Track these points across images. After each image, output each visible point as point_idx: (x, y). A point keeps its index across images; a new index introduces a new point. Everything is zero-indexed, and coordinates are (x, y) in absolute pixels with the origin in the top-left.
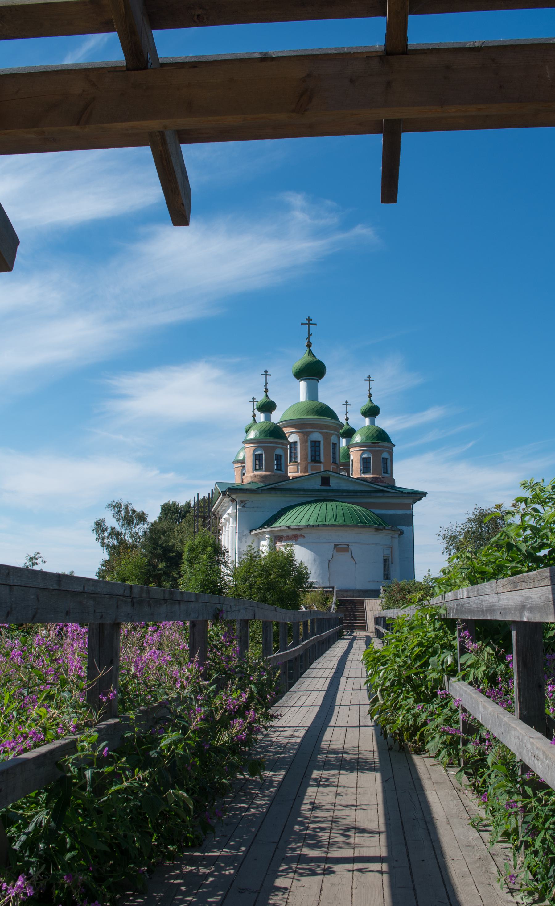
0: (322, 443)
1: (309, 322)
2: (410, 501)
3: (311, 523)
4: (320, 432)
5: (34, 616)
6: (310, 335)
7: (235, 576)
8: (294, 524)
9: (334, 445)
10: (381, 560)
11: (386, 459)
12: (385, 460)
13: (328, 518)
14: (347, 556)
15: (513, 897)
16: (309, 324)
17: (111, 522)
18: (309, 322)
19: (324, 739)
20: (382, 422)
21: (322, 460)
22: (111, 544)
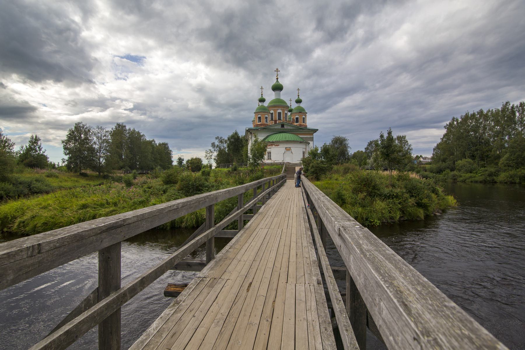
0: (282, 113)
1: (262, 88)
2: (312, 133)
3: (277, 140)
4: (281, 109)
5: (98, 290)
6: (278, 75)
7: (309, 154)
8: (272, 140)
9: (286, 114)
10: (302, 153)
11: (304, 118)
12: (304, 118)
13: (283, 138)
14: (290, 152)
15: (105, 85)
16: (277, 71)
17: (217, 143)
18: (262, 88)
19: (500, 344)
20: (302, 105)
21: (282, 119)
22: (75, 298)
